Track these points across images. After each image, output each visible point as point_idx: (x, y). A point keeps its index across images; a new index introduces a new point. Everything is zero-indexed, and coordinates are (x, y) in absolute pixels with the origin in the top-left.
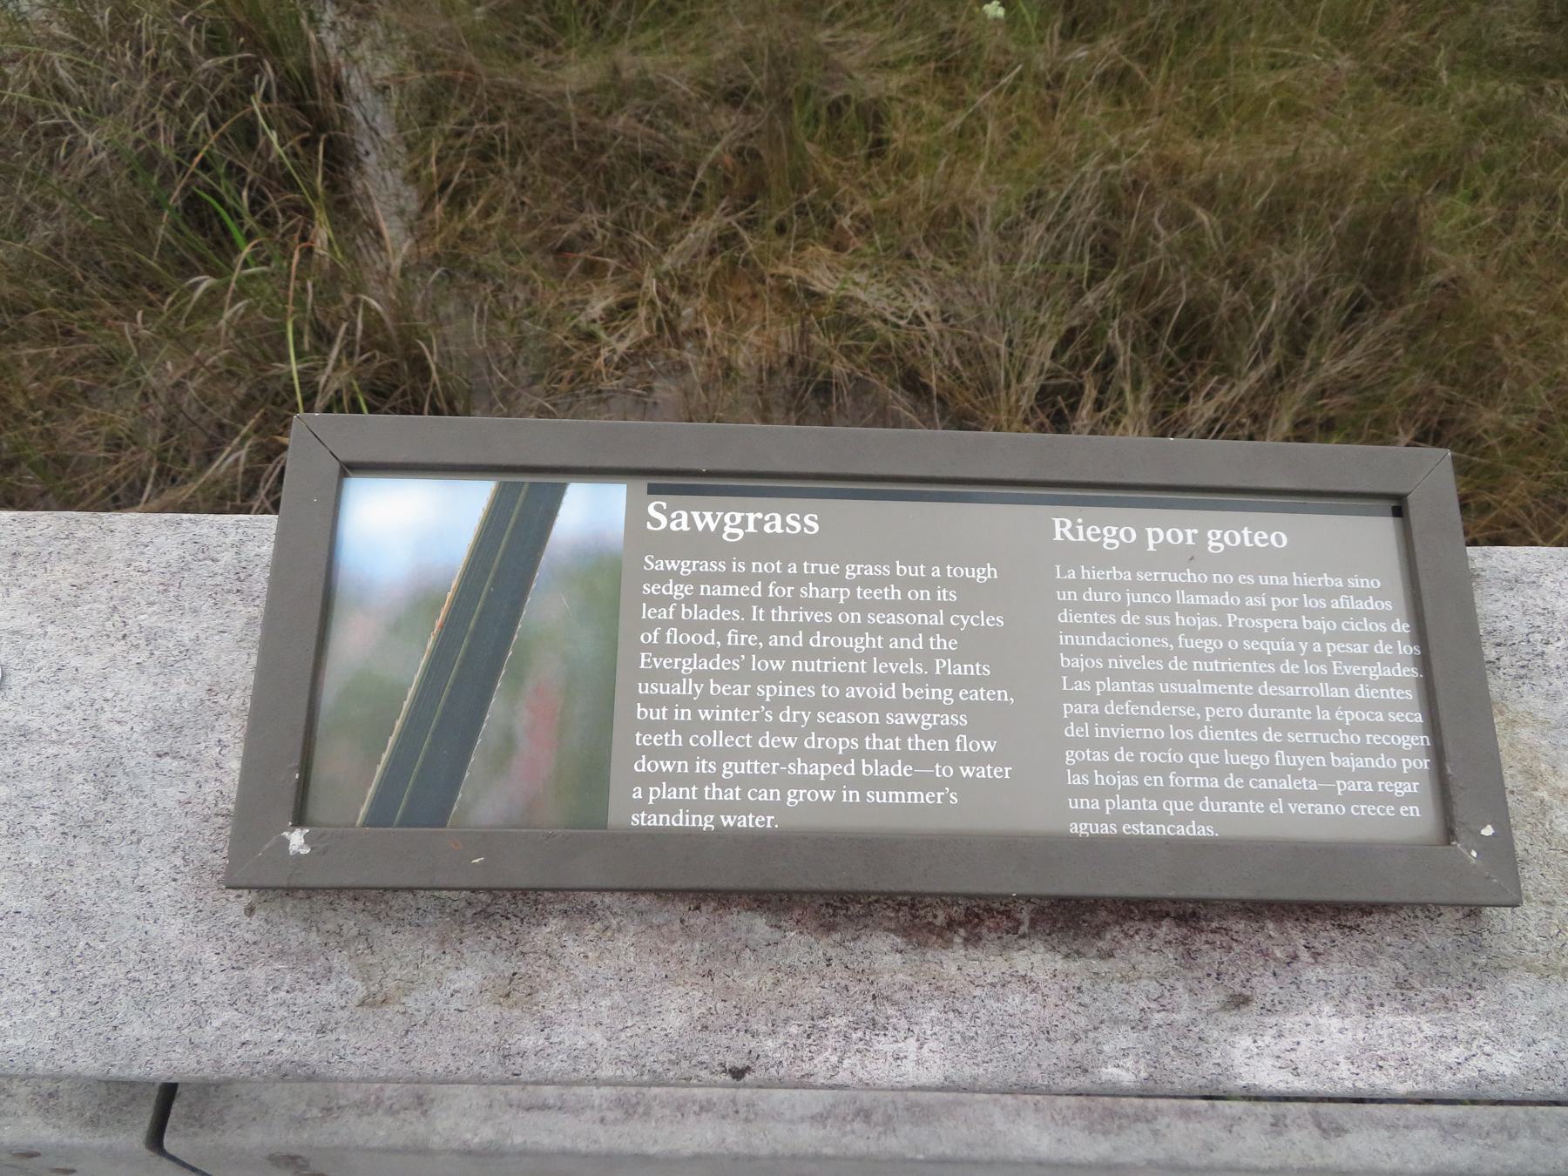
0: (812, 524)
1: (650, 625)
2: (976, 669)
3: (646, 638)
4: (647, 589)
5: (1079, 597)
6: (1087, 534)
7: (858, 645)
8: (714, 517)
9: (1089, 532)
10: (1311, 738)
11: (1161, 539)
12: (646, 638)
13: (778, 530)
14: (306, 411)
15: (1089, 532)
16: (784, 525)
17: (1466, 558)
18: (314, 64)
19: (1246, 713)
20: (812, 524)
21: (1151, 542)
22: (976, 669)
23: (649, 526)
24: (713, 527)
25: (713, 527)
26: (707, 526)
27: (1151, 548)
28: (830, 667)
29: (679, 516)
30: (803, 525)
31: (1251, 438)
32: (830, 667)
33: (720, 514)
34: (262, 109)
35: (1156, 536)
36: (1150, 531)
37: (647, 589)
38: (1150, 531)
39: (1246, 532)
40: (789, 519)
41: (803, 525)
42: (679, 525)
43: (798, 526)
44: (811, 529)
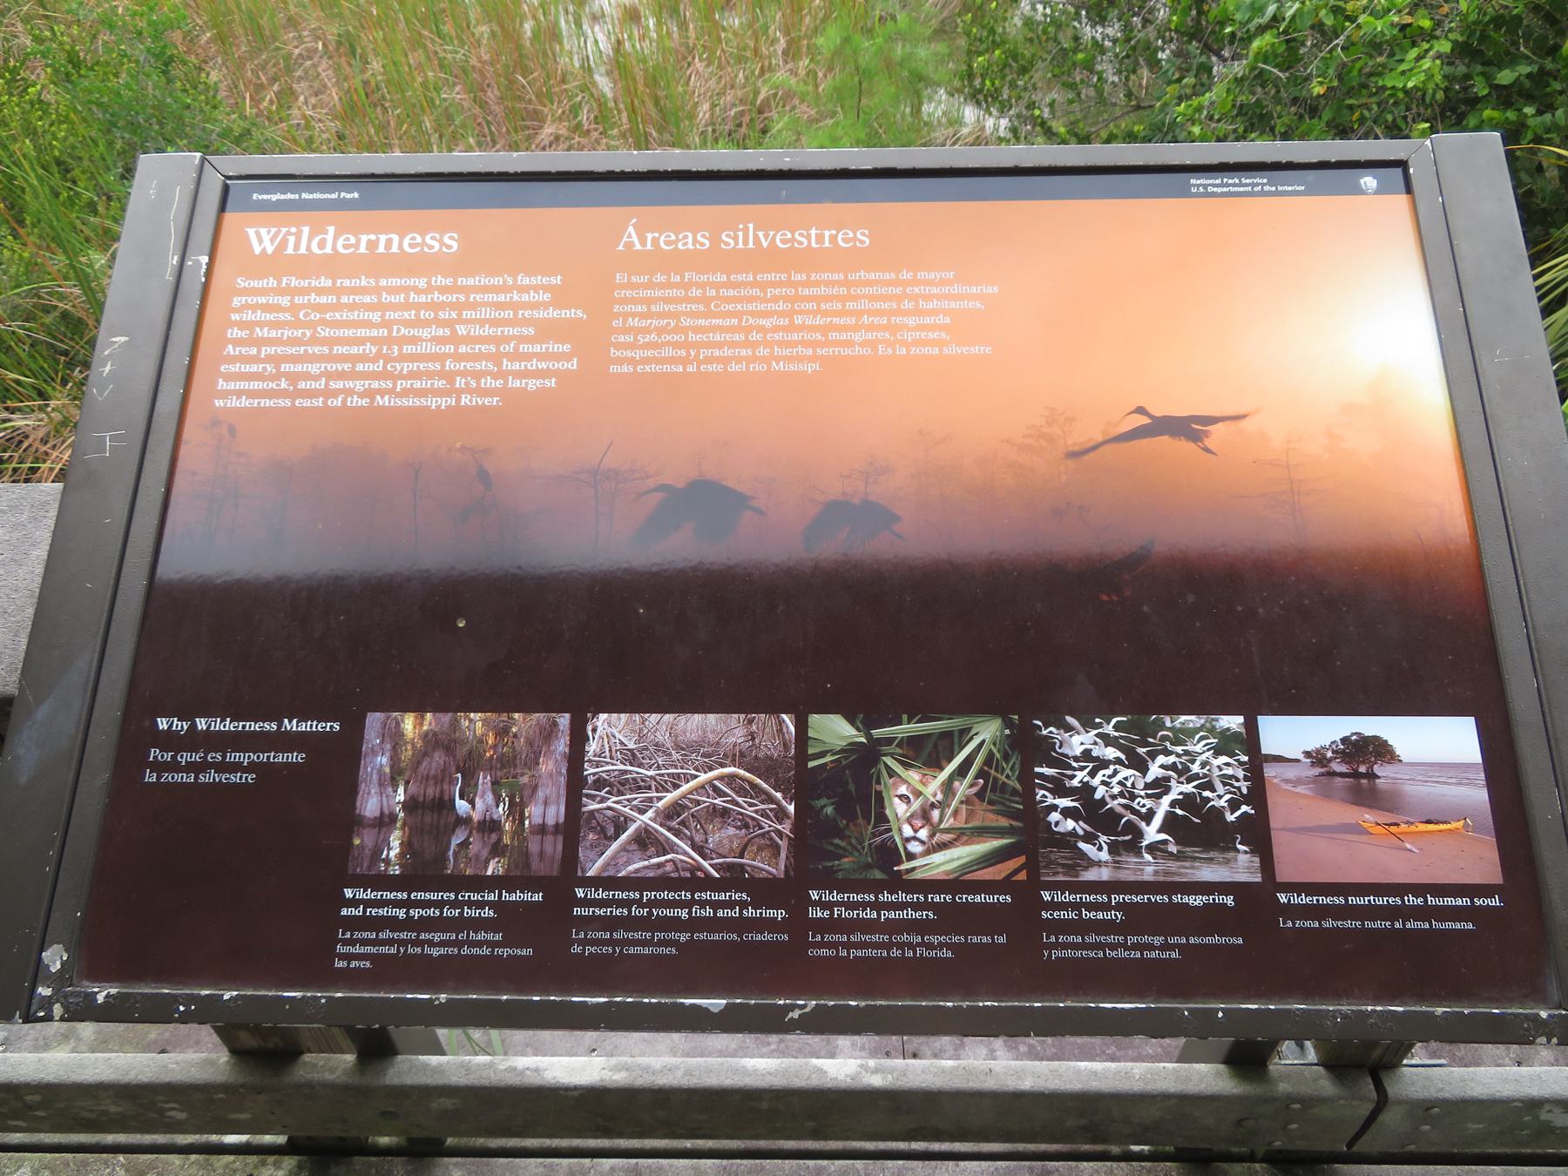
0: (452, 242)
1: (617, 316)
3: (504, 348)
8: (766, 236)
9: (340, 242)
10: (834, 351)
11: (317, 240)
12: (504, 348)
13: (690, 246)
15: (340, 242)
16: (695, 241)
19: (459, 951)
20: (452, 242)
23: (723, 246)
24: (270, 250)
25: (270, 250)
26: (264, 249)
30: (442, 243)
31: (27, 481)
33: (772, 233)
34: (599, 803)
40: (805, 242)
41: (442, 243)
43: (437, 246)
44: (862, 242)
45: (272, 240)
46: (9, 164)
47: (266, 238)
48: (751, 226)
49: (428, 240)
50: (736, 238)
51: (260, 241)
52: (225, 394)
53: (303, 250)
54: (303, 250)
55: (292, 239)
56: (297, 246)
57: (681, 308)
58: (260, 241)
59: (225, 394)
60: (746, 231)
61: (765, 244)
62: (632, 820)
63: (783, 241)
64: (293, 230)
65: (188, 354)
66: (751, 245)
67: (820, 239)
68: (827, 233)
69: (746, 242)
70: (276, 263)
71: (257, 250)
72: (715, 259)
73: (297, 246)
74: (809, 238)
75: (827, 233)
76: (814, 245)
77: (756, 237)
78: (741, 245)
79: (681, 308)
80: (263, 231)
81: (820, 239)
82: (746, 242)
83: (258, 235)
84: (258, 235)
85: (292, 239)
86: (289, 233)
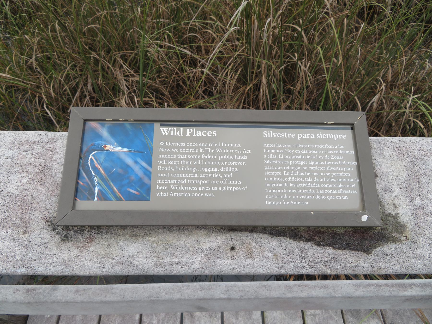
2: (238, 182)
4: (160, 162)
5: (300, 152)
6: (305, 136)
7: (293, 179)
9: (323, 136)
14: (362, 111)
15: (323, 136)
17: (368, 141)
18: (93, 52)
21: (299, 137)
22: (238, 182)
24: (167, 134)
25: (167, 134)
27: (299, 139)
28: (183, 195)
29: (199, 132)
32: (183, 195)
35: (300, 136)
36: (298, 135)
37: (160, 162)
38: (298, 135)
39: (286, 134)
42: (199, 134)
44: (214, 135)
45: (167, 132)
46: (301, 79)
47: (166, 131)
48: (271, 132)
49: (213, 133)
50: (320, 136)
51: (164, 132)
52: (159, 191)
53: (175, 135)
54: (175, 135)
55: (172, 131)
56: (174, 134)
57: (276, 162)
58: (164, 132)
59: (159, 191)
60: (270, 133)
61: (275, 136)
62: (31, 64)
63: (210, 134)
64: (172, 129)
65: (80, 143)
66: (272, 136)
67: (287, 135)
68: (289, 134)
69: (270, 136)
70: (168, 138)
71: (164, 134)
72: (184, 139)
73: (174, 134)
74: (285, 135)
75: (289, 134)
76: (286, 137)
77: (273, 135)
78: (269, 136)
79: (276, 162)
80: (165, 129)
81: (287, 135)
82: (270, 136)
83: (163, 130)
84: (163, 130)
85: (172, 131)
86: (171, 130)
